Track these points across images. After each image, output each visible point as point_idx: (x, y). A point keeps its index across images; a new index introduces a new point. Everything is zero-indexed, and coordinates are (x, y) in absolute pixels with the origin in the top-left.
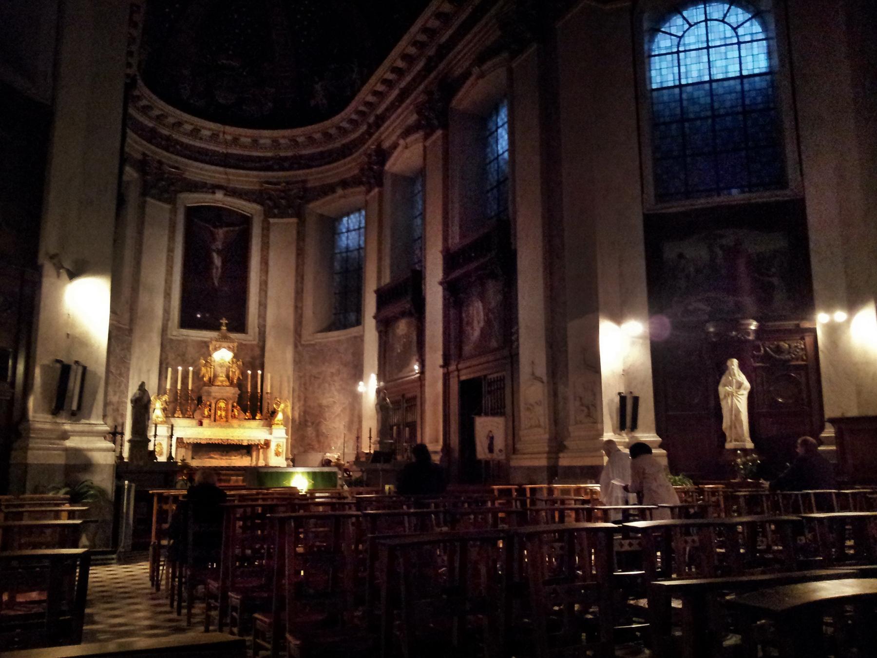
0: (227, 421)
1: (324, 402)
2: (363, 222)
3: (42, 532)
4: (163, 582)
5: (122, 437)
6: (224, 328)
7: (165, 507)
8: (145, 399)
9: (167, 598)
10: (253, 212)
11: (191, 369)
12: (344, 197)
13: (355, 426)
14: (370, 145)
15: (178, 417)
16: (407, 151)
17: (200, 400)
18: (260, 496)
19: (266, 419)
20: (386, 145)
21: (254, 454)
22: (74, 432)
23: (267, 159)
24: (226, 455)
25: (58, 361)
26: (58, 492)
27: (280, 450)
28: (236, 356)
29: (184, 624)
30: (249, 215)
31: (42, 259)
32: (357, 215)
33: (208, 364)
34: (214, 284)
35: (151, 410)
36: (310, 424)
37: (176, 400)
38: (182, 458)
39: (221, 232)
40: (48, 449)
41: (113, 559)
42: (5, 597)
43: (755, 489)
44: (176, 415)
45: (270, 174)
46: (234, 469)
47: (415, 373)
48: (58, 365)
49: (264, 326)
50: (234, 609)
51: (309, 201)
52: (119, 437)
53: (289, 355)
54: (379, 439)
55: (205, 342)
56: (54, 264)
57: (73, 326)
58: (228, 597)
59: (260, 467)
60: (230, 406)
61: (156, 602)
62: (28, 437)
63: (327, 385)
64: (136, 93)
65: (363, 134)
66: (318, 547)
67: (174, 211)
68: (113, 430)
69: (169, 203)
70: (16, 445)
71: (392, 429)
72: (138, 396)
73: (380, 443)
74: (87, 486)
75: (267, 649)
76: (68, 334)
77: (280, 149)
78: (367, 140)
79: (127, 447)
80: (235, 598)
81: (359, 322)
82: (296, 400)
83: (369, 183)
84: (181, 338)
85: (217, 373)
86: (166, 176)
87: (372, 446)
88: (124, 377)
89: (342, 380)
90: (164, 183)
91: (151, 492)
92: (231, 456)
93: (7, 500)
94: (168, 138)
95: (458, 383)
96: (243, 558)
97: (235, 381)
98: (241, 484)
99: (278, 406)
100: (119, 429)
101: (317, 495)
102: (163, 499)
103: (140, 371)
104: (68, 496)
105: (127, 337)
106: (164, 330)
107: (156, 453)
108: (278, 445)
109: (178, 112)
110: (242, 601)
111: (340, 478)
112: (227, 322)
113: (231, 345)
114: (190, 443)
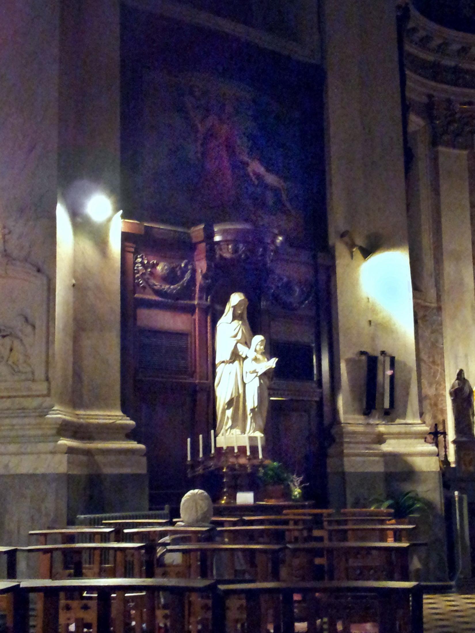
5: (445, 437)
8: (467, 390)
22: (389, 434)
25: (362, 353)
31: (333, 239)
40: (363, 455)
48: (364, 358)
52: (441, 438)
56: (346, 244)
57: (374, 310)
62: (342, 444)
64: (411, 25)
68: (433, 431)
69: (466, 148)
70: (331, 451)
72: (457, 387)
74: (411, 498)
76: (370, 322)
79: (452, 449)
86: (457, 116)
88: (438, 365)
90: (456, 125)
93: (329, 515)
94: (456, 70)
100: (440, 429)
103: (456, 357)
104: (392, 511)
109: (461, 34)
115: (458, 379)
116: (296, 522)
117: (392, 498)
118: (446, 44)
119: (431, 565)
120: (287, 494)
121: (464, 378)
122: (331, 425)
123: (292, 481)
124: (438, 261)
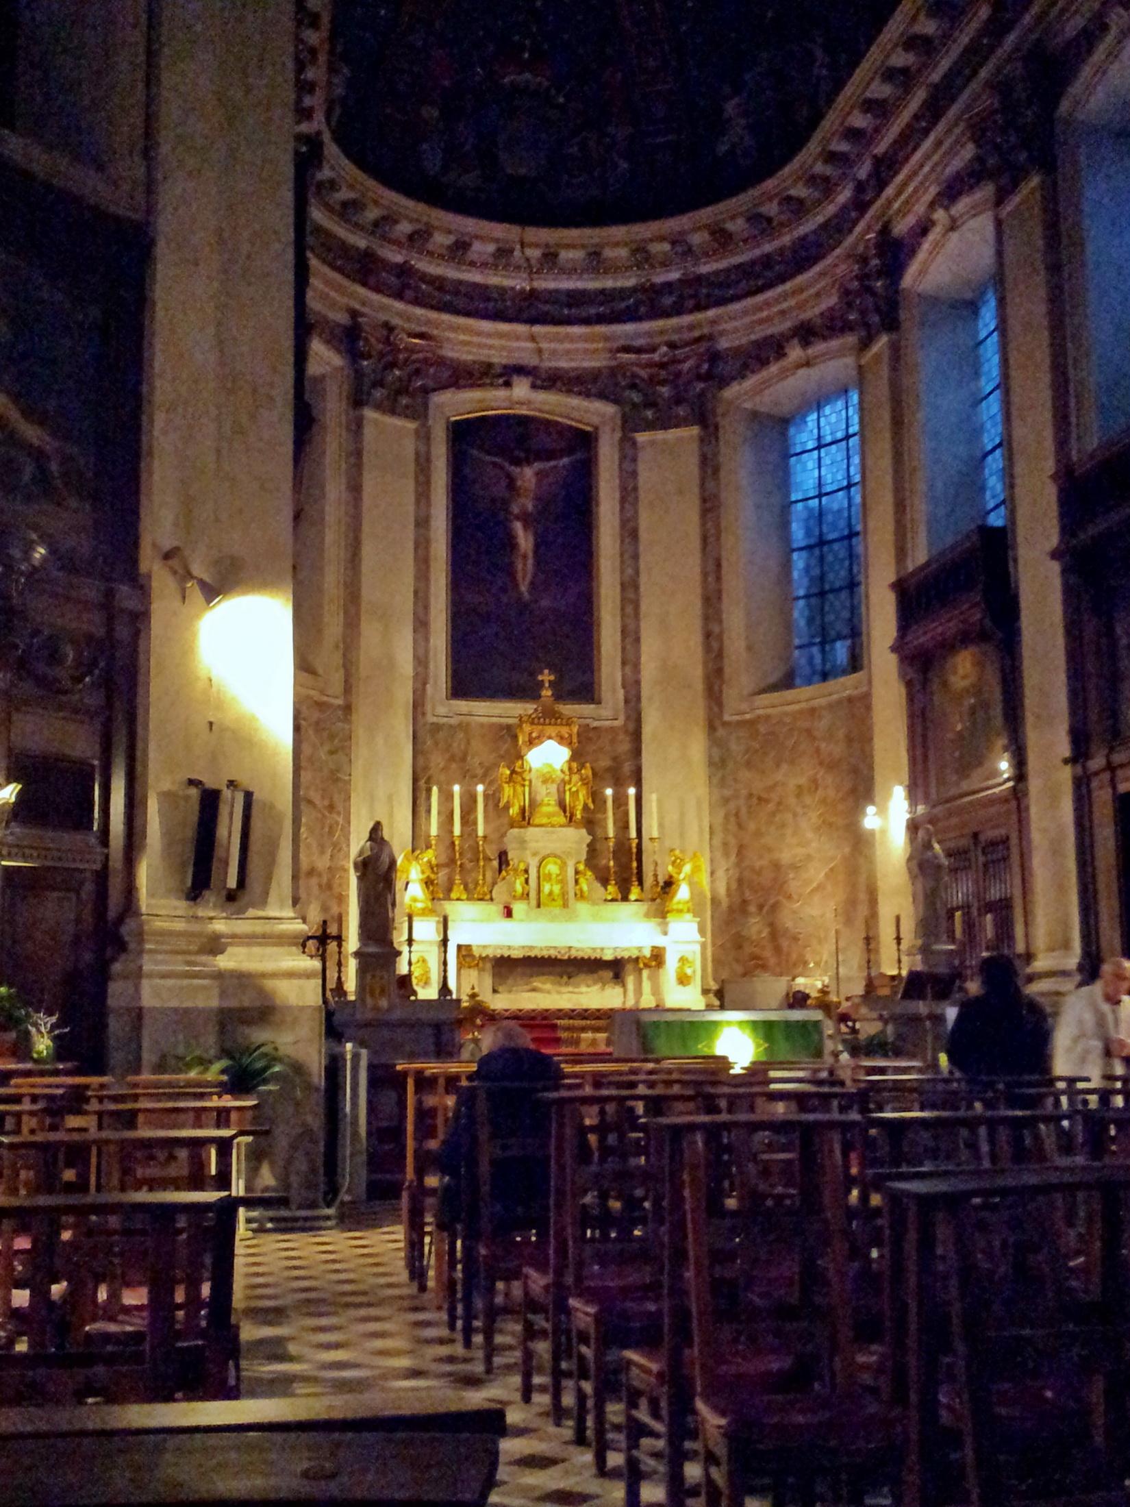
0: (565, 905)
1: (785, 857)
2: (855, 420)
3: (172, 1157)
4: (431, 1273)
5: (340, 946)
6: (547, 693)
7: (430, 1101)
8: (385, 859)
9: (439, 1308)
10: (596, 420)
11: (480, 788)
12: (808, 364)
13: (863, 911)
14: (863, 232)
15: (458, 899)
16: (954, 236)
17: (503, 858)
18: (643, 1077)
19: (653, 900)
20: (901, 228)
21: (630, 980)
22: (234, 936)
23: (622, 293)
24: (567, 984)
25: (192, 782)
26: (206, 1070)
27: (689, 971)
28: (576, 756)
29: (478, 1368)
30: (589, 429)
31: (149, 562)
32: (840, 404)
33: (516, 775)
34: (521, 594)
35: (399, 885)
36: (752, 908)
37: (452, 861)
38: (470, 992)
39: (527, 475)
41: (328, 1218)
42: (102, 1295)
43: (459, 1255)
44: (454, 895)
45: (629, 328)
46: (584, 1014)
47: (1000, 780)
48: (194, 792)
49: (638, 683)
50: (584, 1338)
51: (724, 382)
52: (332, 946)
53: (698, 748)
54: (919, 942)
55: (508, 727)
57: (220, 705)
58: (568, 1311)
59: (644, 1010)
60: (570, 872)
61: (421, 1316)
63: (789, 816)
64: (326, 174)
65: (844, 208)
66: (779, 1198)
67: (424, 436)
70: (117, 967)
71: (951, 917)
72: (368, 853)
73: (925, 950)
74: (265, 1055)
75: (655, 1435)
76: (211, 724)
77: (652, 266)
78: (855, 222)
79: (352, 965)
80: (583, 1312)
81: (856, 663)
82: (718, 854)
83: (867, 326)
84: (454, 721)
85: (539, 798)
87: (905, 959)
89: (823, 801)
91: (399, 1068)
92: (577, 986)
93: (102, 1086)
94: (404, 271)
95: (1114, 801)
96: (605, 1220)
97: (579, 815)
98: (602, 1048)
99: (678, 865)
100: (332, 930)
101: (773, 1074)
102: (425, 1083)
103: (372, 798)
104: (225, 1078)
105: (340, 724)
106: (418, 705)
107: (414, 981)
108: (683, 960)
109: (421, 207)
110: (598, 1319)
111: (830, 1037)
112: (552, 678)
113: (565, 731)
114: (487, 956)
115: (371, 839)
116: (34, 1099)
117: (232, 1058)
118: (389, 219)
119: (294, 1180)
120: (22, 1048)
121: (382, 839)
122: (120, 920)
123: (36, 1025)
124: (352, 623)
